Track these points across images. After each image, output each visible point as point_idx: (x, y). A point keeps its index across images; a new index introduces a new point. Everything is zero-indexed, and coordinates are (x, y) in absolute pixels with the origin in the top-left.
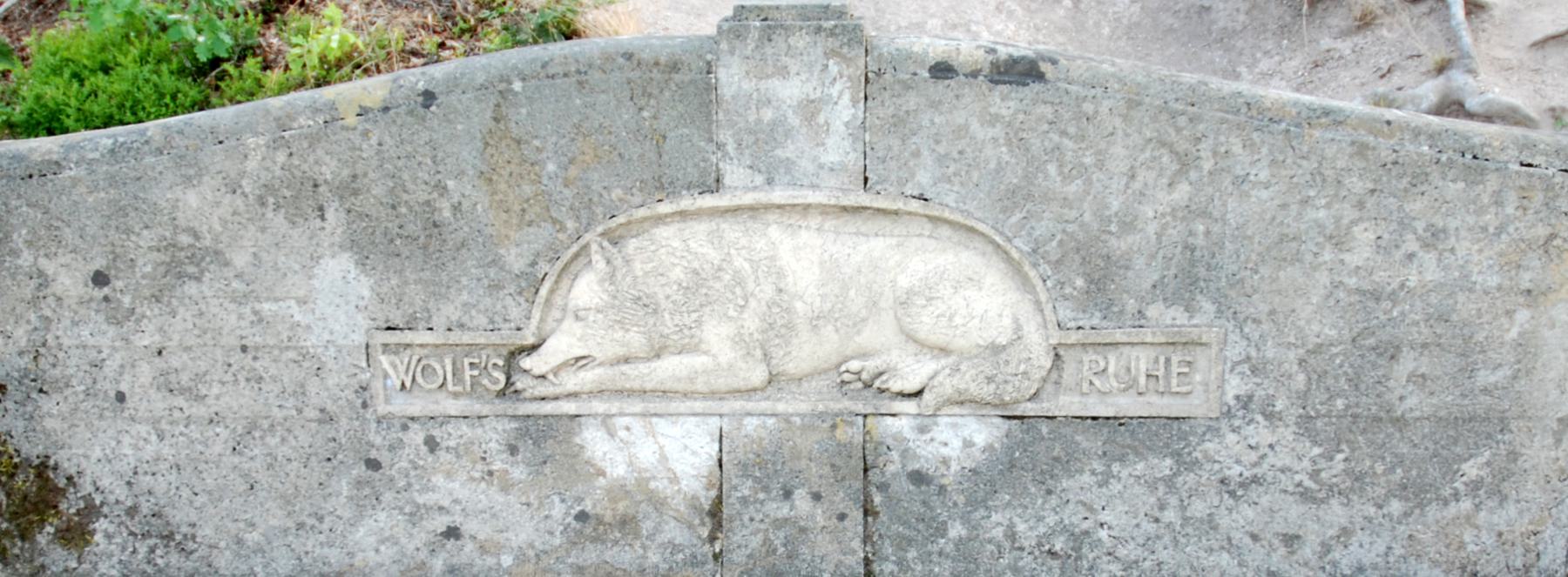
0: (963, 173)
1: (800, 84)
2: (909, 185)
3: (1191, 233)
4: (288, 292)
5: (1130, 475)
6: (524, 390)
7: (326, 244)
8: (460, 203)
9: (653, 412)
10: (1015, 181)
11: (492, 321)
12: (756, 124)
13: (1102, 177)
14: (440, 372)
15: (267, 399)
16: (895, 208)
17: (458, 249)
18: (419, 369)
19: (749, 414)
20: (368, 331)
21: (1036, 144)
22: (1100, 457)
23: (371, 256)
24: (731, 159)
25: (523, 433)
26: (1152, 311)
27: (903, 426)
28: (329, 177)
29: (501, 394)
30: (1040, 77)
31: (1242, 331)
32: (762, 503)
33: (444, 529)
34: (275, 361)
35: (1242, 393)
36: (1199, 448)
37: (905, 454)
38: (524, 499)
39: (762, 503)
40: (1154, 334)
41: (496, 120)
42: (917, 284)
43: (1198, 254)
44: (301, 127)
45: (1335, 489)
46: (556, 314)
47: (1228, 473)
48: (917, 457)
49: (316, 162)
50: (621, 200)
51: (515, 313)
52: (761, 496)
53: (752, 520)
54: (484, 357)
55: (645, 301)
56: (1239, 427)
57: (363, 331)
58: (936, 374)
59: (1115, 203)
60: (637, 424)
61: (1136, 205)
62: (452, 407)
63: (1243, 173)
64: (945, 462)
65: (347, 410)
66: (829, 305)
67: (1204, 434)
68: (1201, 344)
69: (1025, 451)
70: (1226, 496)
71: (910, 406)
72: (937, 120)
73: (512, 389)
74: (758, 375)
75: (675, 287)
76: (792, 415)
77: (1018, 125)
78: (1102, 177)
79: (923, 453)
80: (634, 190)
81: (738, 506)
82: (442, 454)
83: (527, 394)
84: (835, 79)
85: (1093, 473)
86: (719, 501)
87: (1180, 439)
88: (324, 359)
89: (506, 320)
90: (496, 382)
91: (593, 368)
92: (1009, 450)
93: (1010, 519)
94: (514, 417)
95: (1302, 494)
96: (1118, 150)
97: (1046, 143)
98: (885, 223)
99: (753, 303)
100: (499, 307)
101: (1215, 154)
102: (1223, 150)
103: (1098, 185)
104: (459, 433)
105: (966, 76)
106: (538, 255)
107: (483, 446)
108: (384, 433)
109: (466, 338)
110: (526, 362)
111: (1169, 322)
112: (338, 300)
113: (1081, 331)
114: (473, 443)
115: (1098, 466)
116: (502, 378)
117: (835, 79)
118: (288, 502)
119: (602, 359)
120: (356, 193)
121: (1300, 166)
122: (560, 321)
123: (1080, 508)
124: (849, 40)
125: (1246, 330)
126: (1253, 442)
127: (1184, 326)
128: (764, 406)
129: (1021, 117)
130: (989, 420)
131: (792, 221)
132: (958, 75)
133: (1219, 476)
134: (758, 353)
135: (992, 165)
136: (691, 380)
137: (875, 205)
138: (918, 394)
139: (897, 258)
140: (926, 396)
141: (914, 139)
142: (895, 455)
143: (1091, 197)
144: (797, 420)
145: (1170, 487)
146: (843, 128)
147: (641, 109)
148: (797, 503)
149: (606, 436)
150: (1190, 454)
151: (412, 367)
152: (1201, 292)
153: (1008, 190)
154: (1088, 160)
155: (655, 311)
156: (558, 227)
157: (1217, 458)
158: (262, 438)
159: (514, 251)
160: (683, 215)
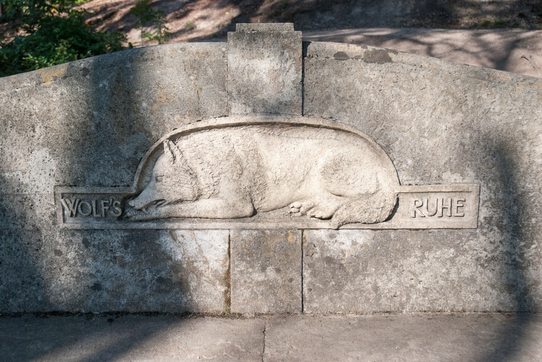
0: (352, 107)
1: (270, 62)
2: (325, 113)
3: (463, 137)
4: (17, 168)
5: (434, 257)
6: (131, 216)
7: (35, 144)
8: (100, 123)
9: (195, 228)
10: (378, 111)
11: (115, 182)
12: (248, 82)
13: (420, 109)
14: (90, 207)
15: (7, 220)
16: (318, 124)
17: (99, 146)
18: (79, 206)
19: (244, 229)
20: (55, 187)
21: (388, 93)
22: (419, 249)
23: (57, 150)
24: (235, 100)
25: (130, 238)
26: (445, 176)
27: (322, 235)
28: (37, 111)
29: (120, 218)
30: (390, 60)
31: (487, 185)
32: (251, 273)
33: (93, 285)
34: (11, 201)
35: (488, 216)
36: (467, 243)
37: (323, 249)
38: (131, 271)
39: (251, 273)
40: (446, 187)
41: (118, 81)
42: (330, 163)
43: (466, 147)
44: (25, 87)
45: (531, 262)
46: (148, 179)
47: (480, 255)
48: (328, 250)
49: (31, 103)
50: (179, 121)
51: (127, 178)
52: (250, 270)
53: (245, 282)
54: (111, 200)
55: (191, 172)
56: (486, 233)
57: (53, 187)
58: (338, 208)
59: (426, 122)
60: (187, 234)
61: (437, 123)
62: (96, 225)
63: (488, 108)
64: (343, 252)
65: (45, 226)
66: (284, 174)
67: (469, 236)
68: (468, 192)
69: (383, 246)
70: (479, 267)
71: (325, 224)
72: (338, 80)
73: (125, 216)
74: (248, 210)
75: (206, 165)
76: (266, 230)
77: (378, 83)
78: (420, 109)
79: (332, 248)
80: (186, 116)
81: (238, 275)
82: (91, 248)
83: (133, 219)
84: (287, 59)
85: (416, 256)
86: (228, 272)
87: (458, 239)
88: (34, 201)
89: (122, 182)
90: (118, 213)
91: (165, 206)
92: (375, 246)
93: (375, 280)
94: (126, 230)
95: (515, 265)
96: (428, 96)
97: (393, 92)
98: (312, 132)
99: (246, 173)
100: (118, 175)
101: (474, 98)
102: (478, 96)
103: (419, 113)
104: (100, 238)
105: (353, 59)
106: (137, 148)
107: (111, 244)
108: (63, 237)
109: (102, 190)
110: (132, 203)
111: (453, 181)
112: (40, 172)
113: (411, 186)
114: (106, 243)
115: (418, 253)
116: (120, 211)
117: (287, 59)
118: (17, 270)
119: (170, 201)
120: (49, 119)
121: (514, 105)
122: (149, 182)
123: (409, 274)
124: (295, 40)
125: (490, 185)
126: (492, 240)
127: (460, 183)
128: (252, 225)
129: (380, 79)
130: (364, 231)
131: (265, 131)
132: (348, 58)
133: (476, 257)
134: (248, 198)
135: (367, 103)
136: (215, 212)
137: (308, 123)
138: (330, 218)
139: (319, 149)
140: (333, 219)
141: (327, 90)
142: (318, 249)
143: (415, 119)
144: (268, 232)
145: (453, 263)
146: (291, 84)
147: (189, 75)
148: (268, 273)
149: (172, 240)
150: (462, 246)
151: (76, 205)
152: (468, 166)
153: (374, 115)
154: (413, 101)
155: (196, 177)
156: (148, 135)
157: (475, 248)
158: (5, 239)
159: (126, 147)
160: (210, 128)
